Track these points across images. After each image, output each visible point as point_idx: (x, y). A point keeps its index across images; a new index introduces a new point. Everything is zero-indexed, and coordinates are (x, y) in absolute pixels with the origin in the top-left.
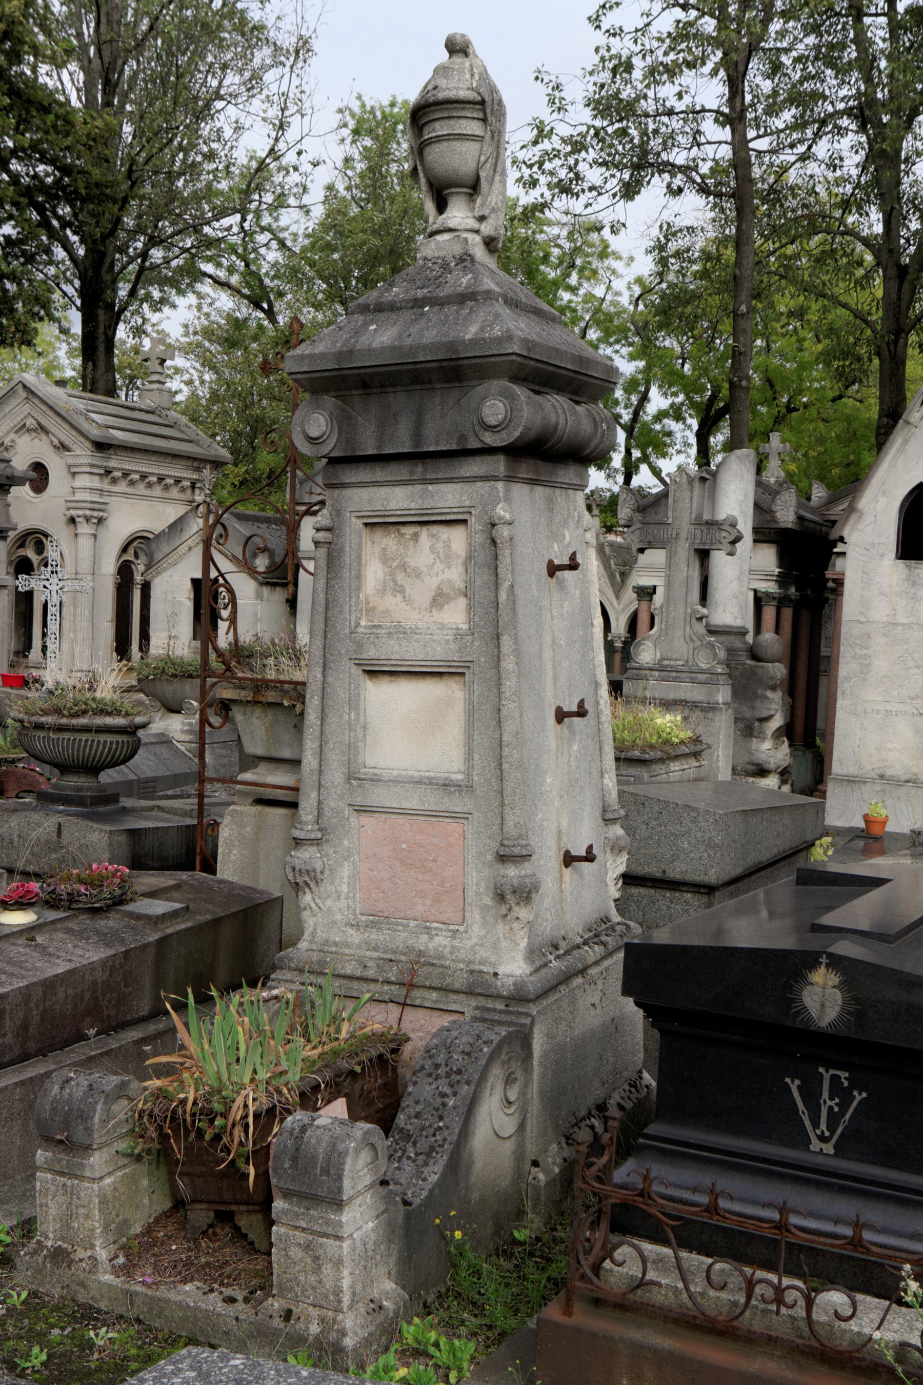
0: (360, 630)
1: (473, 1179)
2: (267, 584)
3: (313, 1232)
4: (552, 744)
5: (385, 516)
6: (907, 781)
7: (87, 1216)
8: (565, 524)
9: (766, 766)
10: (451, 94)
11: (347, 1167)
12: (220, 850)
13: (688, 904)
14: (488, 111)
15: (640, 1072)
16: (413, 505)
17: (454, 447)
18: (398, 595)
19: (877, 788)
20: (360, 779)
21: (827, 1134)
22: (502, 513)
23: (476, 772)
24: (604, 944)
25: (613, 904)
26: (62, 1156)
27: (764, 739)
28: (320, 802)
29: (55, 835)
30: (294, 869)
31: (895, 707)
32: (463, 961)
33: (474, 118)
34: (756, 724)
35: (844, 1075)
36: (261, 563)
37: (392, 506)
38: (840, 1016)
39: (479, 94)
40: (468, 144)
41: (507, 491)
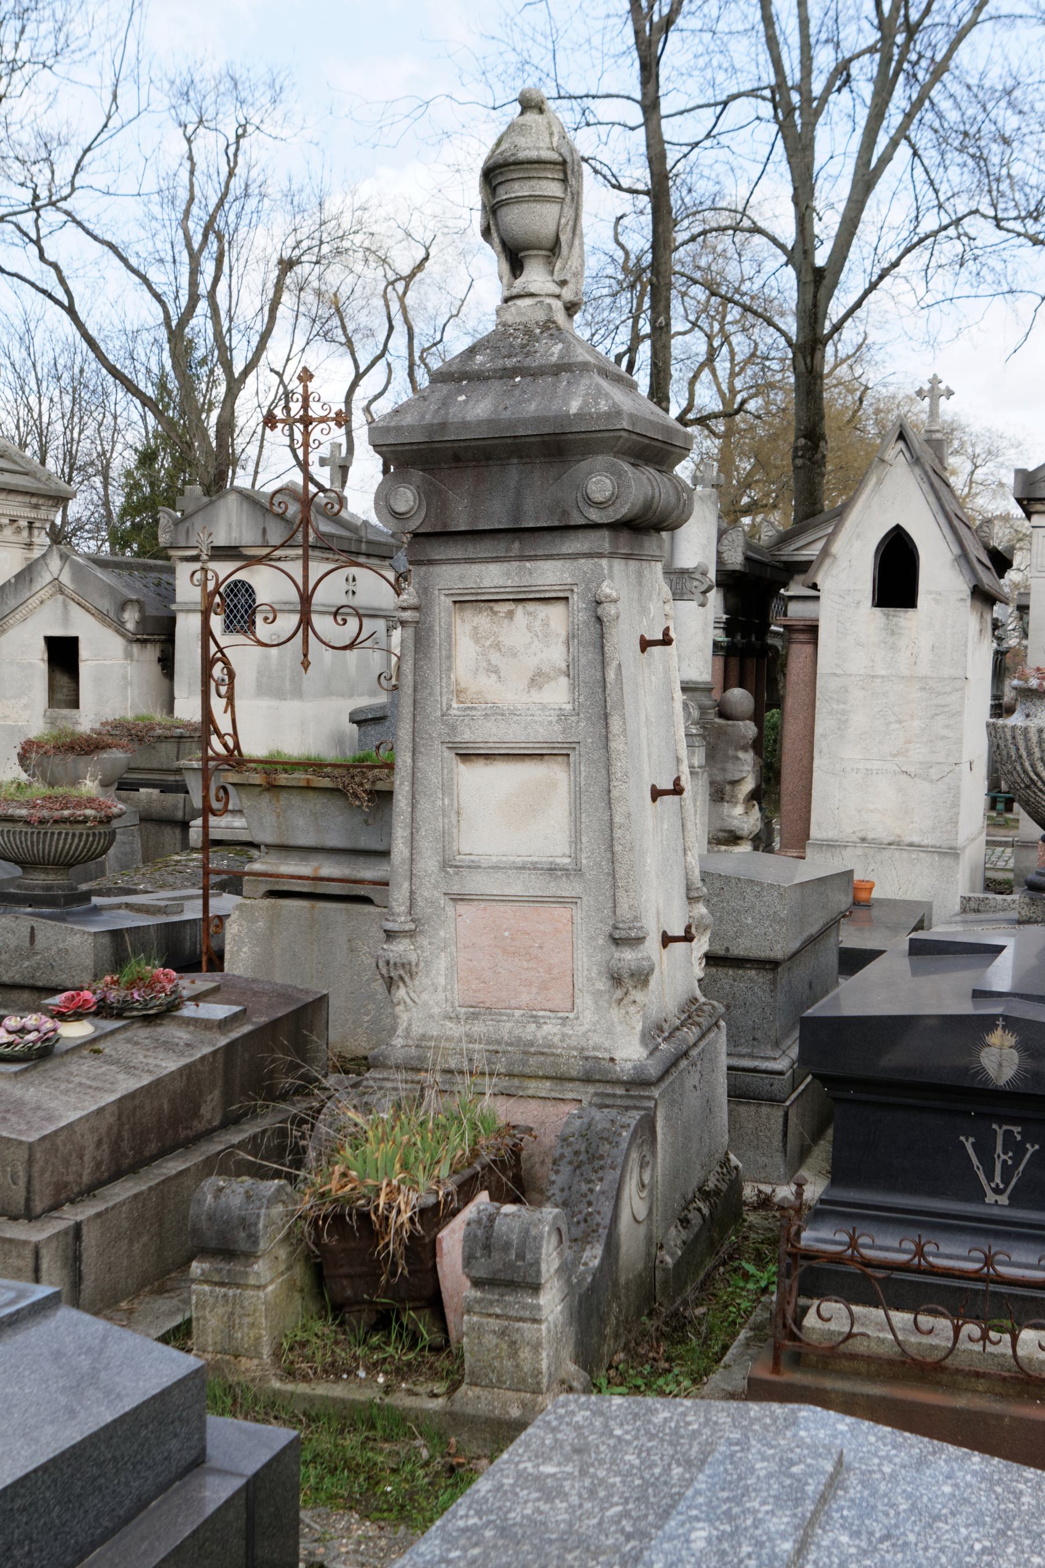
0: (453, 712)
1: (621, 1263)
2: (138, 640)
3: (509, 1318)
4: (650, 824)
5: (477, 594)
6: (890, 844)
7: (252, 1325)
8: (650, 599)
9: (739, 833)
10: (533, 154)
11: (544, 1251)
12: (227, 948)
13: (751, 979)
14: (569, 172)
15: (727, 1154)
16: (509, 583)
17: (556, 524)
18: (493, 675)
19: (859, 852)
20: (456, 867)
21: (1001, 1186)
22: (608, 591)
23: (584, 855)
24: (699, 1025)
25: (696, 984)
26: (222, 1265)
27: (736, 803)
28: (412, 892)
29: (27, 944)
30: (388, 963)
31: (876, 765)
32: (575, 1048)
33: (553, 179)
34: (728, 787)
35: (1016, 1129)
36: (131, 618)
37: (487, 583)
38: (1017, 1075)
39: (561, 154)
40: (548, 205)
41: (611, 567)
